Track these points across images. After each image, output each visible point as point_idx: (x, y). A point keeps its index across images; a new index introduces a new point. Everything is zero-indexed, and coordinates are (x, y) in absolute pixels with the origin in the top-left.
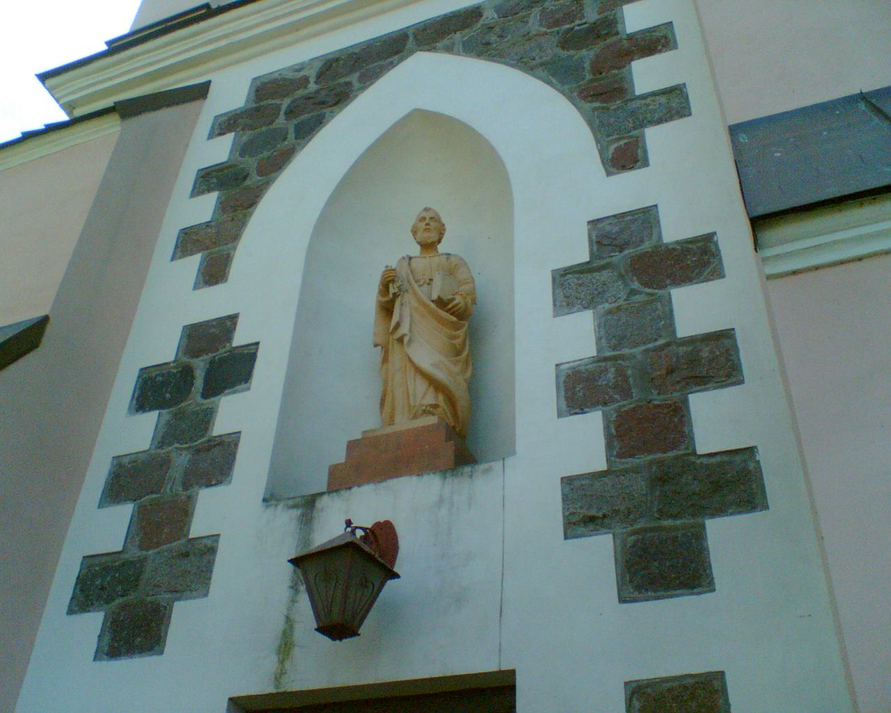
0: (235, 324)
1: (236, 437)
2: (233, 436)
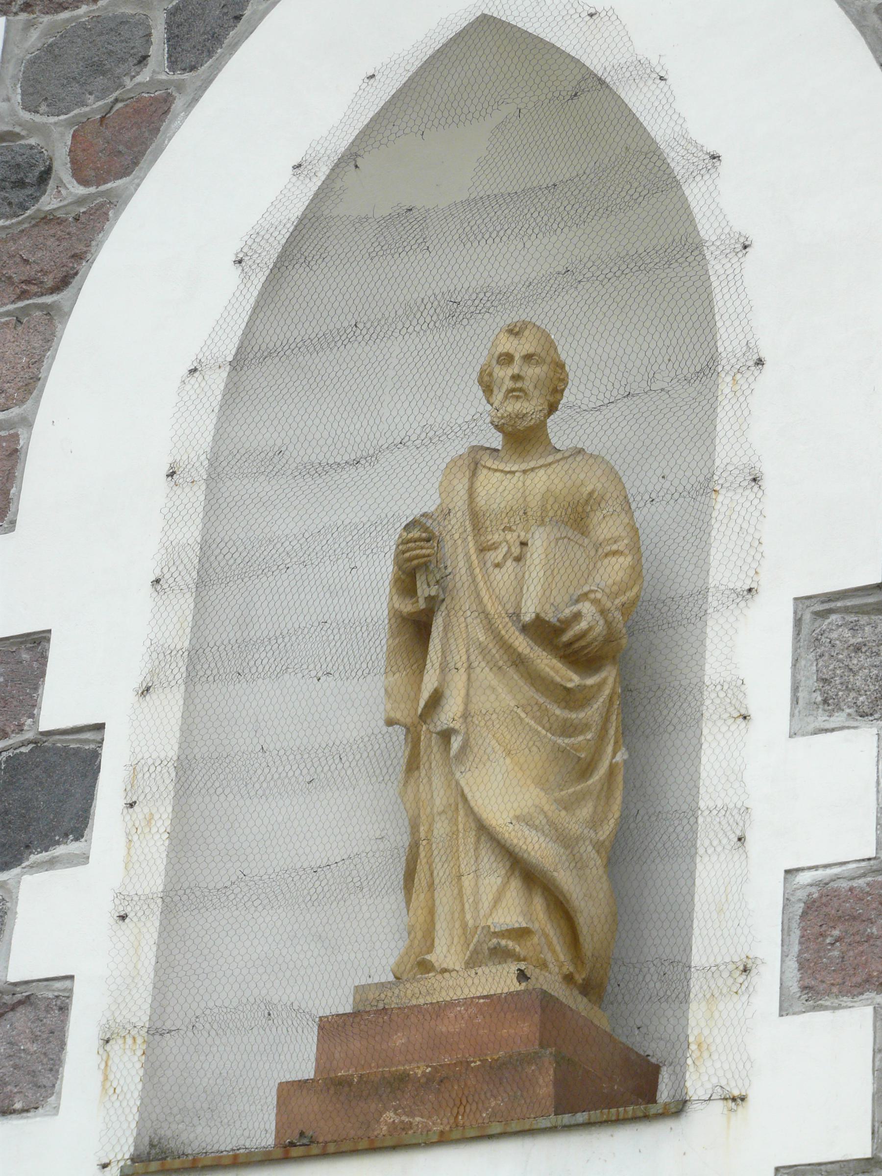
0: (43, 659)
1: (64, 990)
2: (58, 985)
